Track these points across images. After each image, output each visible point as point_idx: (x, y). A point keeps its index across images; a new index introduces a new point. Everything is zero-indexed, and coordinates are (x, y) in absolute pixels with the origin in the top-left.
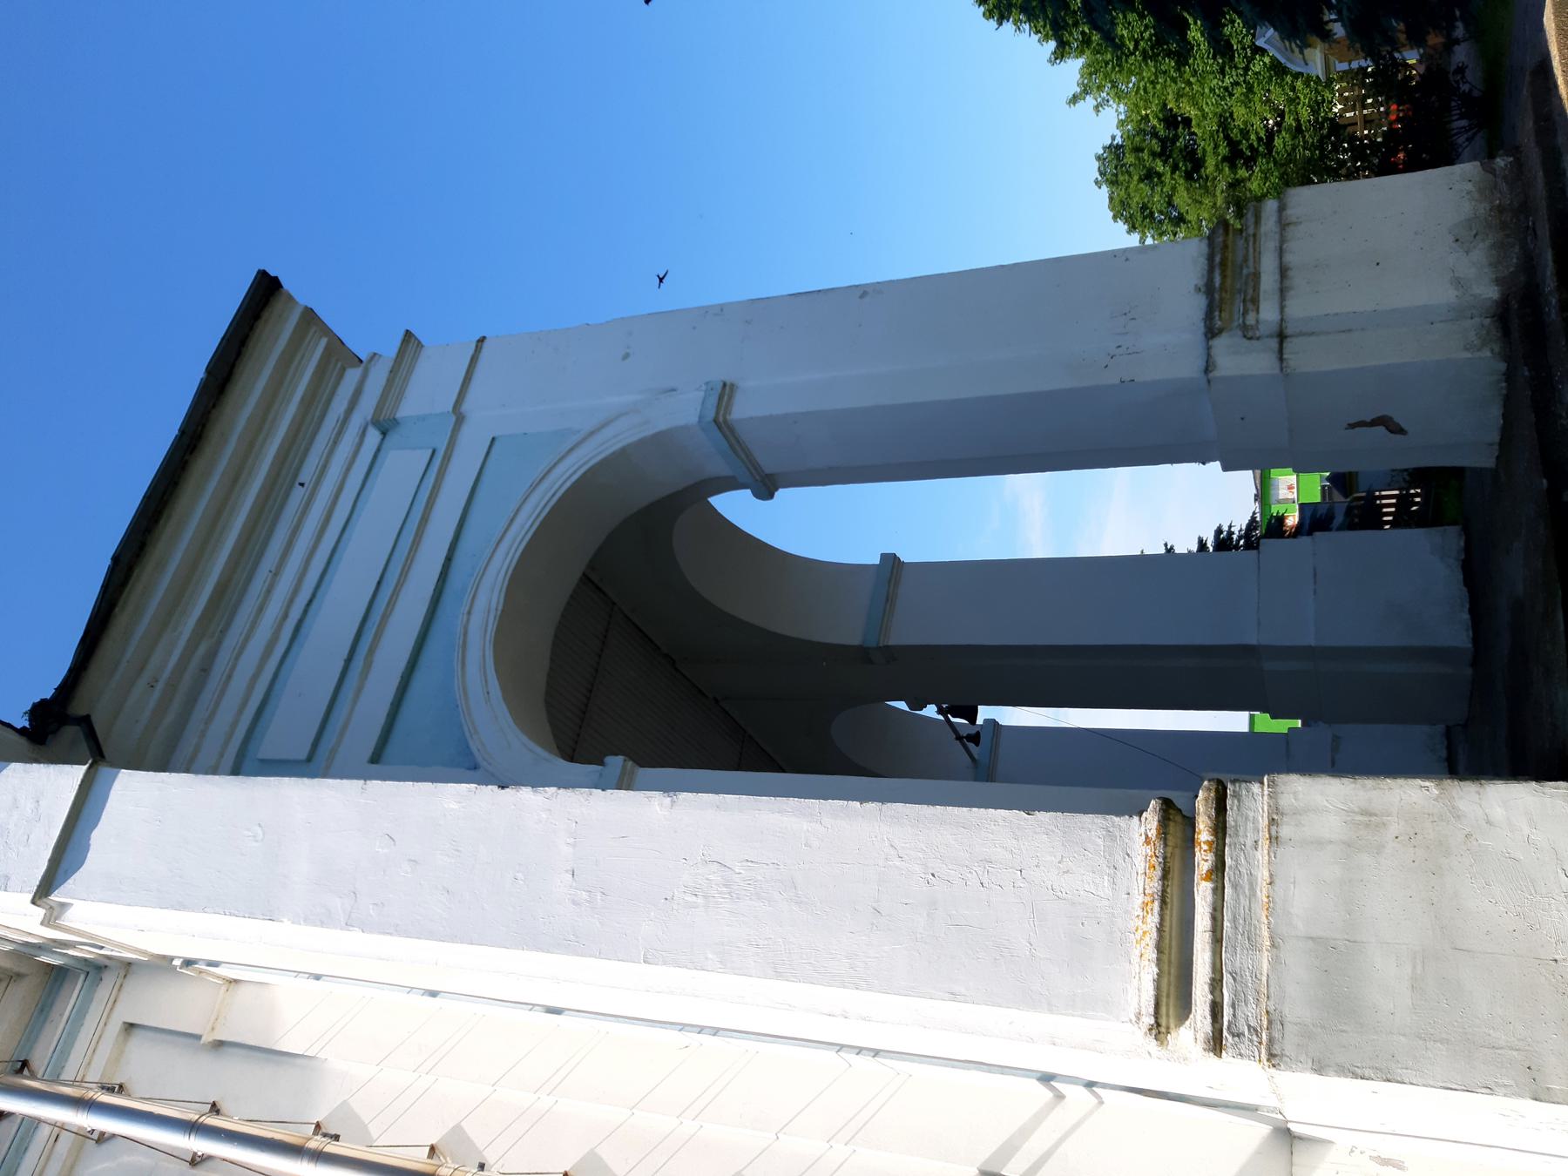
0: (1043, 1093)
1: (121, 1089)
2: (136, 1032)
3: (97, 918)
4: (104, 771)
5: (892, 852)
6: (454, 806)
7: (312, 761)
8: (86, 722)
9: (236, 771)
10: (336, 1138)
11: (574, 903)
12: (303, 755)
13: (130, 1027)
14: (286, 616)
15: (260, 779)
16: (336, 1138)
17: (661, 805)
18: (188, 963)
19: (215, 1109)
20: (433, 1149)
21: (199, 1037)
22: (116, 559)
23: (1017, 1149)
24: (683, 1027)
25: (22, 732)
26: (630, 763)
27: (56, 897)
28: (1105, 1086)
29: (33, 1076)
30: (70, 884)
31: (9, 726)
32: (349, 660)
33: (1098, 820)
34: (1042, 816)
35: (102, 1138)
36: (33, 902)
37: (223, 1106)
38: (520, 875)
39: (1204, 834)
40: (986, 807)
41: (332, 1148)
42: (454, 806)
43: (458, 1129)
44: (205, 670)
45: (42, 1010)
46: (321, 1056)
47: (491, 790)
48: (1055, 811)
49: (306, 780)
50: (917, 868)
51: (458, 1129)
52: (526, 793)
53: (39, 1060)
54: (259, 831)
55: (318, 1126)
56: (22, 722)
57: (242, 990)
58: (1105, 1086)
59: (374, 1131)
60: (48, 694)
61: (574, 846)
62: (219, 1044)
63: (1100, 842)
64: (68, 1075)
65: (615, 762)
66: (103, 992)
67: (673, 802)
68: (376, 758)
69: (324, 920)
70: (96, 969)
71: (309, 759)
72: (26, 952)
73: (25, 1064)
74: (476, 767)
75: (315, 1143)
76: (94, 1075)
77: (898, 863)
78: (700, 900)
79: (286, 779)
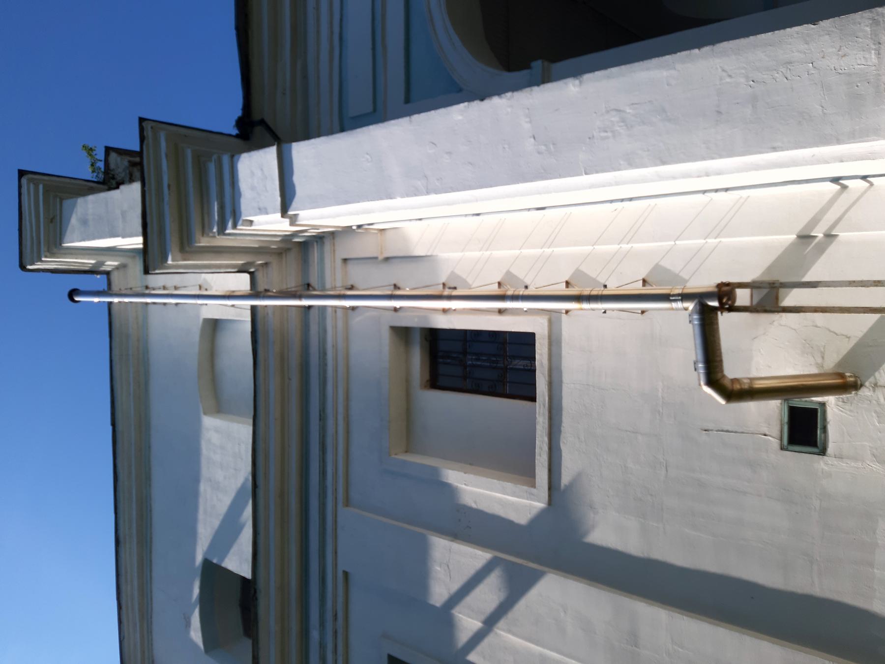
0: (836, 187)
1: (352, 288)
2: (349, 262)
3: (314, 217)
4: (285, 146)
5: (724, 74)
6: (460, 118)
7: (376, 114)
8: (262, 122)
9: (342, 130)
10: (455, 288)
11: (539, 153)
12: (370, 109)
13: (345, 260)
14: (332, 33)
15: (359, 130)
16: (455, 288)
17: (574, 85)
18: (359, 227)
19: (396, 287)
20: (499, 284)
21: (376, 258)
22: (237, 28)
23: (819, 220)
24: (612, 201)
25: (237, 136)
26: (546, 63)
27: (290, 213)
28: (874, 176)
29: (314, 290)
30: (294, 204)
31: (230, 135)
32: (374, 48)
33: (866, 14)
34: (825, 24)
35: (353, 308)
36: (282, 216)
37: (399, 285)
38: (506, 146)
39: (149, 300)
40: (784, 28)
41: (455, 293)
42: (460, 118)
43: (508, 273)
44: (305, 77)
45: (305, 262)
46: (434, 254)
47: (476, 104)
48: (834, 17)
49: (381, 125)
50: (742, 80)
51: (508, 273)
52: (496, 101)
53: (314, 281)
54: (368, 157)
55: (444, 285)
56: (235, 132)
57: (388, 232)
58: (874, 176)
59: (470, 282)
60: (239, 113)
61: (530, 122)
62: (387, 259)
63: (868, 29)
64: (328, 286)
65: (537, 65)
66: (327, 247)
67: (581, 82)
68: (407, 100)
69: (416, 193)
70: (321, 238)
71: (375, 110)
72: (287, 239)
73: (309, 285)
74: (460, 90)
75: (447, 292)
76: (339, 284)
77: (728, 80)
78: (609, 134)
79: (371, 127)
